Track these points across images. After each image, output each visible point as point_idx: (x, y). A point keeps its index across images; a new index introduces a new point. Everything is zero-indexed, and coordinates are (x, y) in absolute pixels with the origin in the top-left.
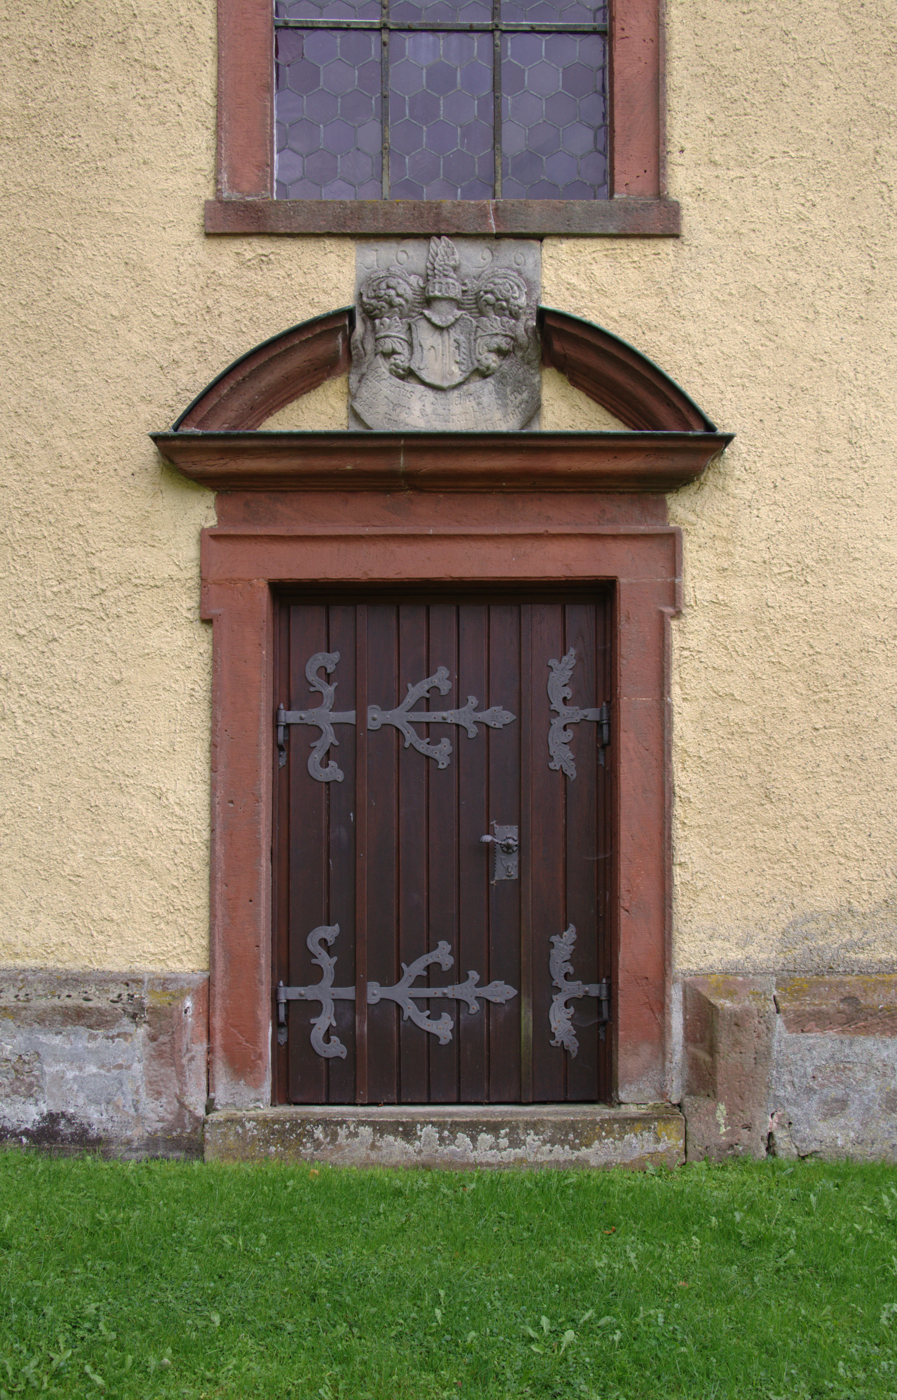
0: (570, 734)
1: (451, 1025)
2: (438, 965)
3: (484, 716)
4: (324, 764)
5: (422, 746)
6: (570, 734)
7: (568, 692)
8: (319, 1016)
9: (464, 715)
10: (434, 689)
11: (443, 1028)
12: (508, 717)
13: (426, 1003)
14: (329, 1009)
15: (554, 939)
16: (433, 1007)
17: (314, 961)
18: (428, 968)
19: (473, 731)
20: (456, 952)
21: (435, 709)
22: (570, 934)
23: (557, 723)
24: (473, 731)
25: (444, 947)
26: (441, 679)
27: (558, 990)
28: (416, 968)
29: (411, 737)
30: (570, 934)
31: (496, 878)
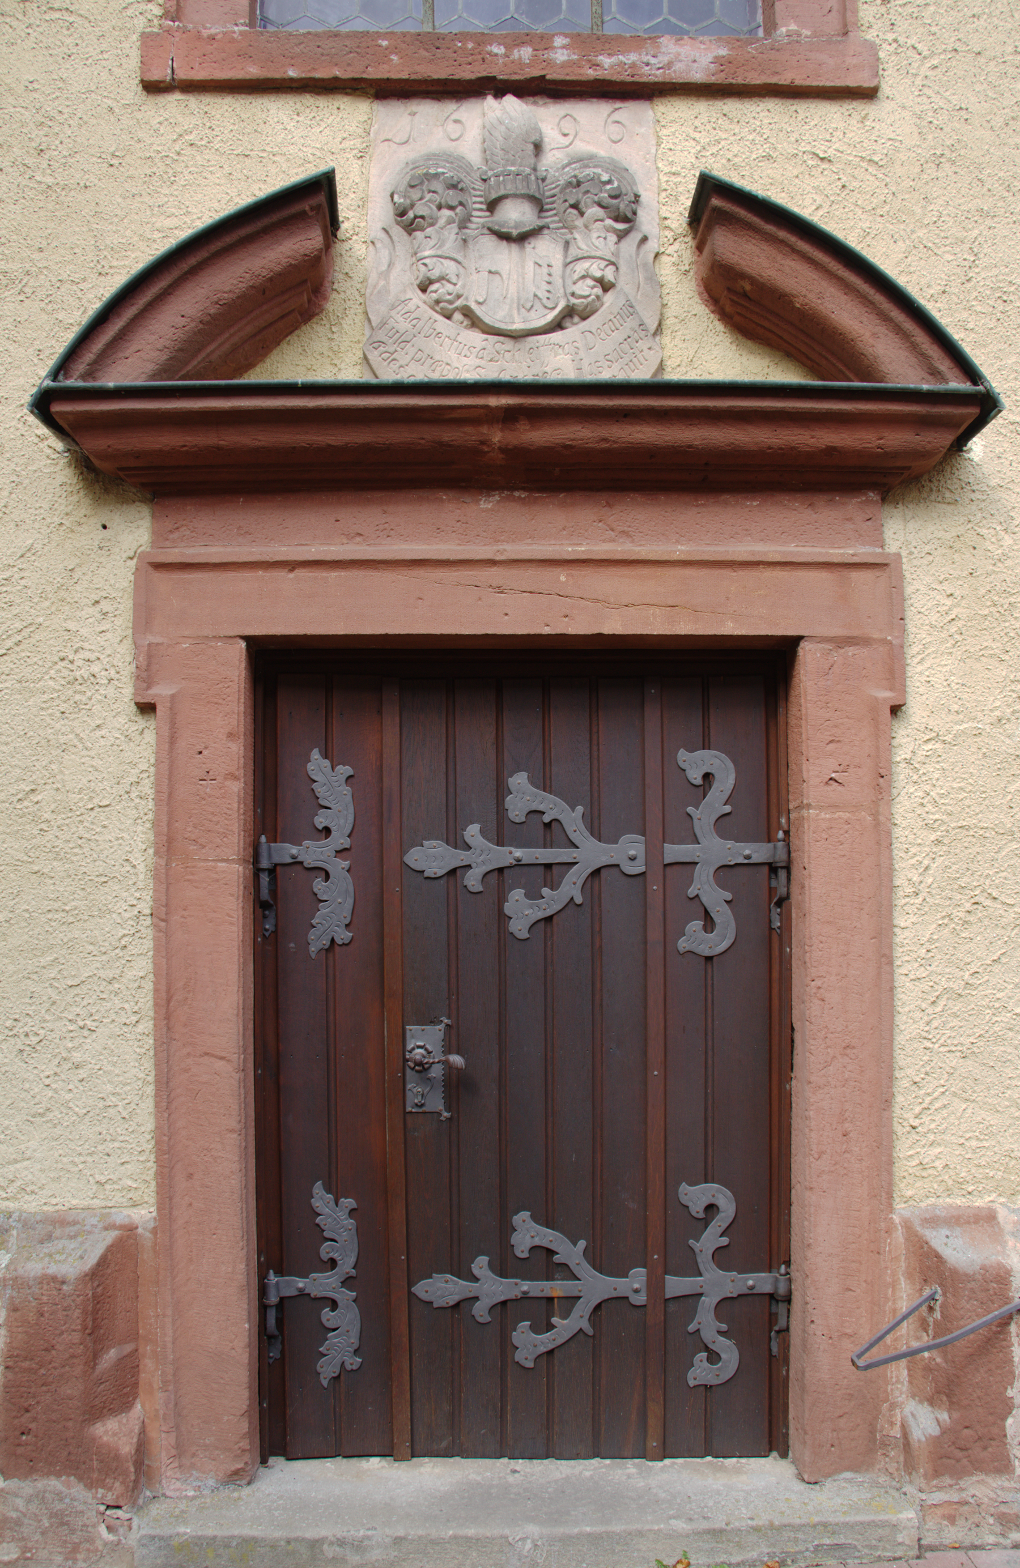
0: (321, 820)
1: (515, 1239)
2: (536, 1329)
3: (456, 858)
4: (711, 1209)
5: (553, 807)
6: (326, 1251)
7: (327, 1316)
8: (721, 837)
9: (491, 1287)
10: (534, 895)
11: (528, 1233)
12: (423, 1289)
13: (551, 831)
14: (704, 1260)
15: (354, 1362)
16: (545, 1263)
17: (729, 896)
18: (550, 1327)
19: (473, 832)
20: (506, 1347)
21: (535, 835)
22: (327, 1370)
23: (340, 839)
24: (473, 832)
25: (519, 927)
26: (522, 911)
27: (347, 1282)
28: (565, 1327)
29: (573, 820)
30: (327, 1370)
31: (442, 1027)
